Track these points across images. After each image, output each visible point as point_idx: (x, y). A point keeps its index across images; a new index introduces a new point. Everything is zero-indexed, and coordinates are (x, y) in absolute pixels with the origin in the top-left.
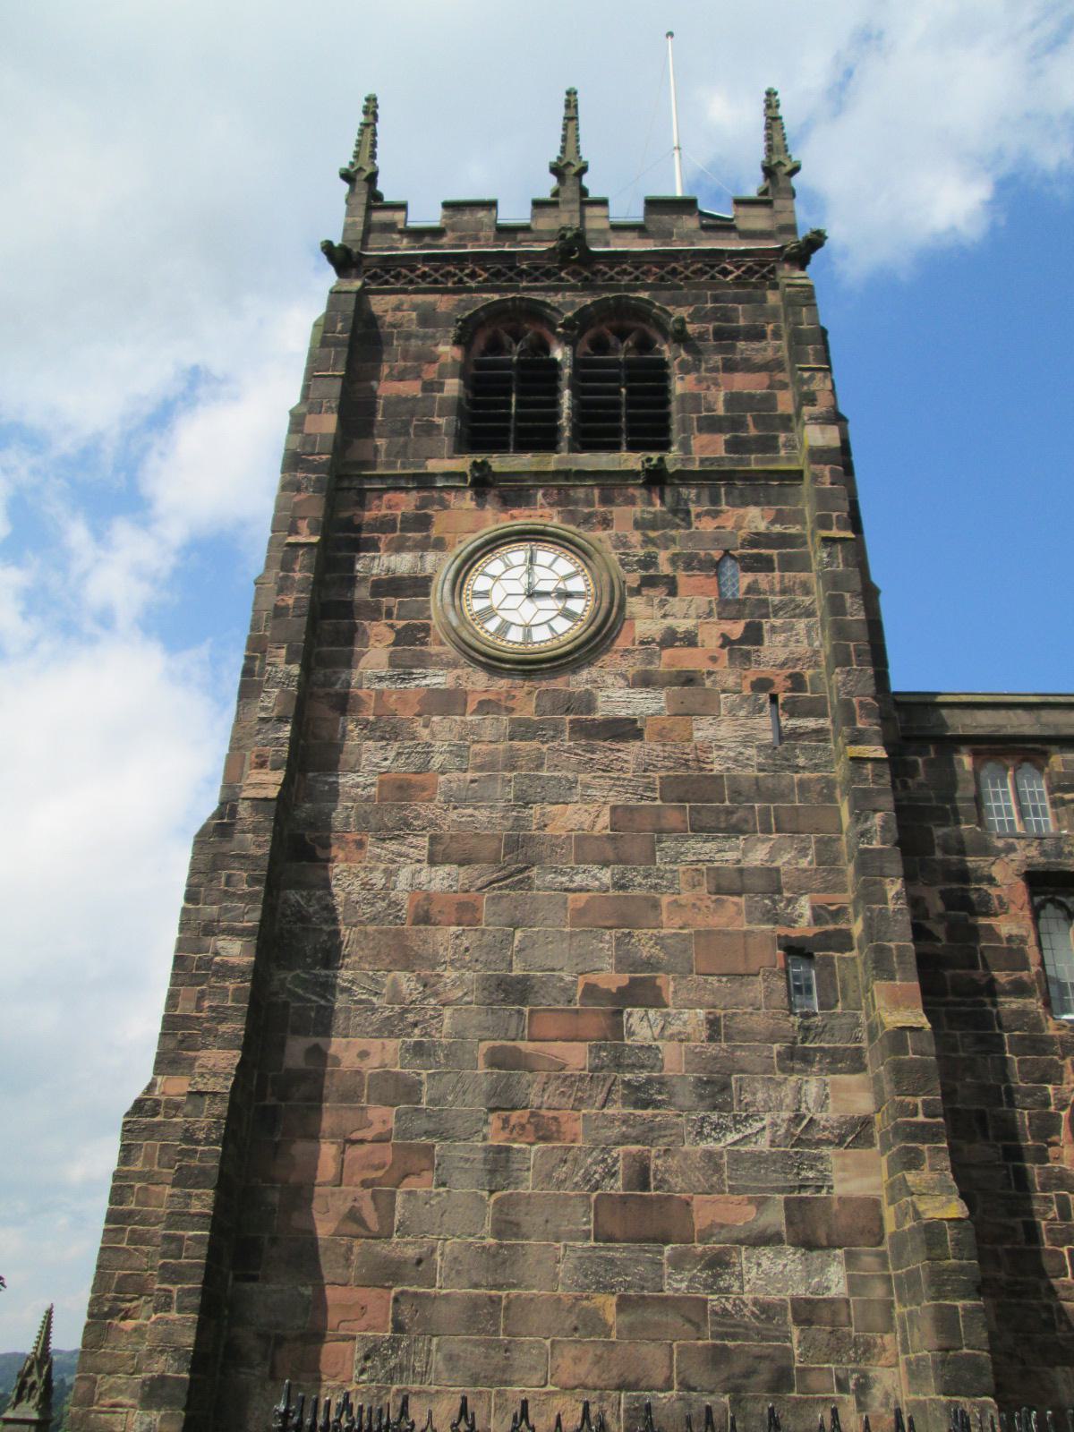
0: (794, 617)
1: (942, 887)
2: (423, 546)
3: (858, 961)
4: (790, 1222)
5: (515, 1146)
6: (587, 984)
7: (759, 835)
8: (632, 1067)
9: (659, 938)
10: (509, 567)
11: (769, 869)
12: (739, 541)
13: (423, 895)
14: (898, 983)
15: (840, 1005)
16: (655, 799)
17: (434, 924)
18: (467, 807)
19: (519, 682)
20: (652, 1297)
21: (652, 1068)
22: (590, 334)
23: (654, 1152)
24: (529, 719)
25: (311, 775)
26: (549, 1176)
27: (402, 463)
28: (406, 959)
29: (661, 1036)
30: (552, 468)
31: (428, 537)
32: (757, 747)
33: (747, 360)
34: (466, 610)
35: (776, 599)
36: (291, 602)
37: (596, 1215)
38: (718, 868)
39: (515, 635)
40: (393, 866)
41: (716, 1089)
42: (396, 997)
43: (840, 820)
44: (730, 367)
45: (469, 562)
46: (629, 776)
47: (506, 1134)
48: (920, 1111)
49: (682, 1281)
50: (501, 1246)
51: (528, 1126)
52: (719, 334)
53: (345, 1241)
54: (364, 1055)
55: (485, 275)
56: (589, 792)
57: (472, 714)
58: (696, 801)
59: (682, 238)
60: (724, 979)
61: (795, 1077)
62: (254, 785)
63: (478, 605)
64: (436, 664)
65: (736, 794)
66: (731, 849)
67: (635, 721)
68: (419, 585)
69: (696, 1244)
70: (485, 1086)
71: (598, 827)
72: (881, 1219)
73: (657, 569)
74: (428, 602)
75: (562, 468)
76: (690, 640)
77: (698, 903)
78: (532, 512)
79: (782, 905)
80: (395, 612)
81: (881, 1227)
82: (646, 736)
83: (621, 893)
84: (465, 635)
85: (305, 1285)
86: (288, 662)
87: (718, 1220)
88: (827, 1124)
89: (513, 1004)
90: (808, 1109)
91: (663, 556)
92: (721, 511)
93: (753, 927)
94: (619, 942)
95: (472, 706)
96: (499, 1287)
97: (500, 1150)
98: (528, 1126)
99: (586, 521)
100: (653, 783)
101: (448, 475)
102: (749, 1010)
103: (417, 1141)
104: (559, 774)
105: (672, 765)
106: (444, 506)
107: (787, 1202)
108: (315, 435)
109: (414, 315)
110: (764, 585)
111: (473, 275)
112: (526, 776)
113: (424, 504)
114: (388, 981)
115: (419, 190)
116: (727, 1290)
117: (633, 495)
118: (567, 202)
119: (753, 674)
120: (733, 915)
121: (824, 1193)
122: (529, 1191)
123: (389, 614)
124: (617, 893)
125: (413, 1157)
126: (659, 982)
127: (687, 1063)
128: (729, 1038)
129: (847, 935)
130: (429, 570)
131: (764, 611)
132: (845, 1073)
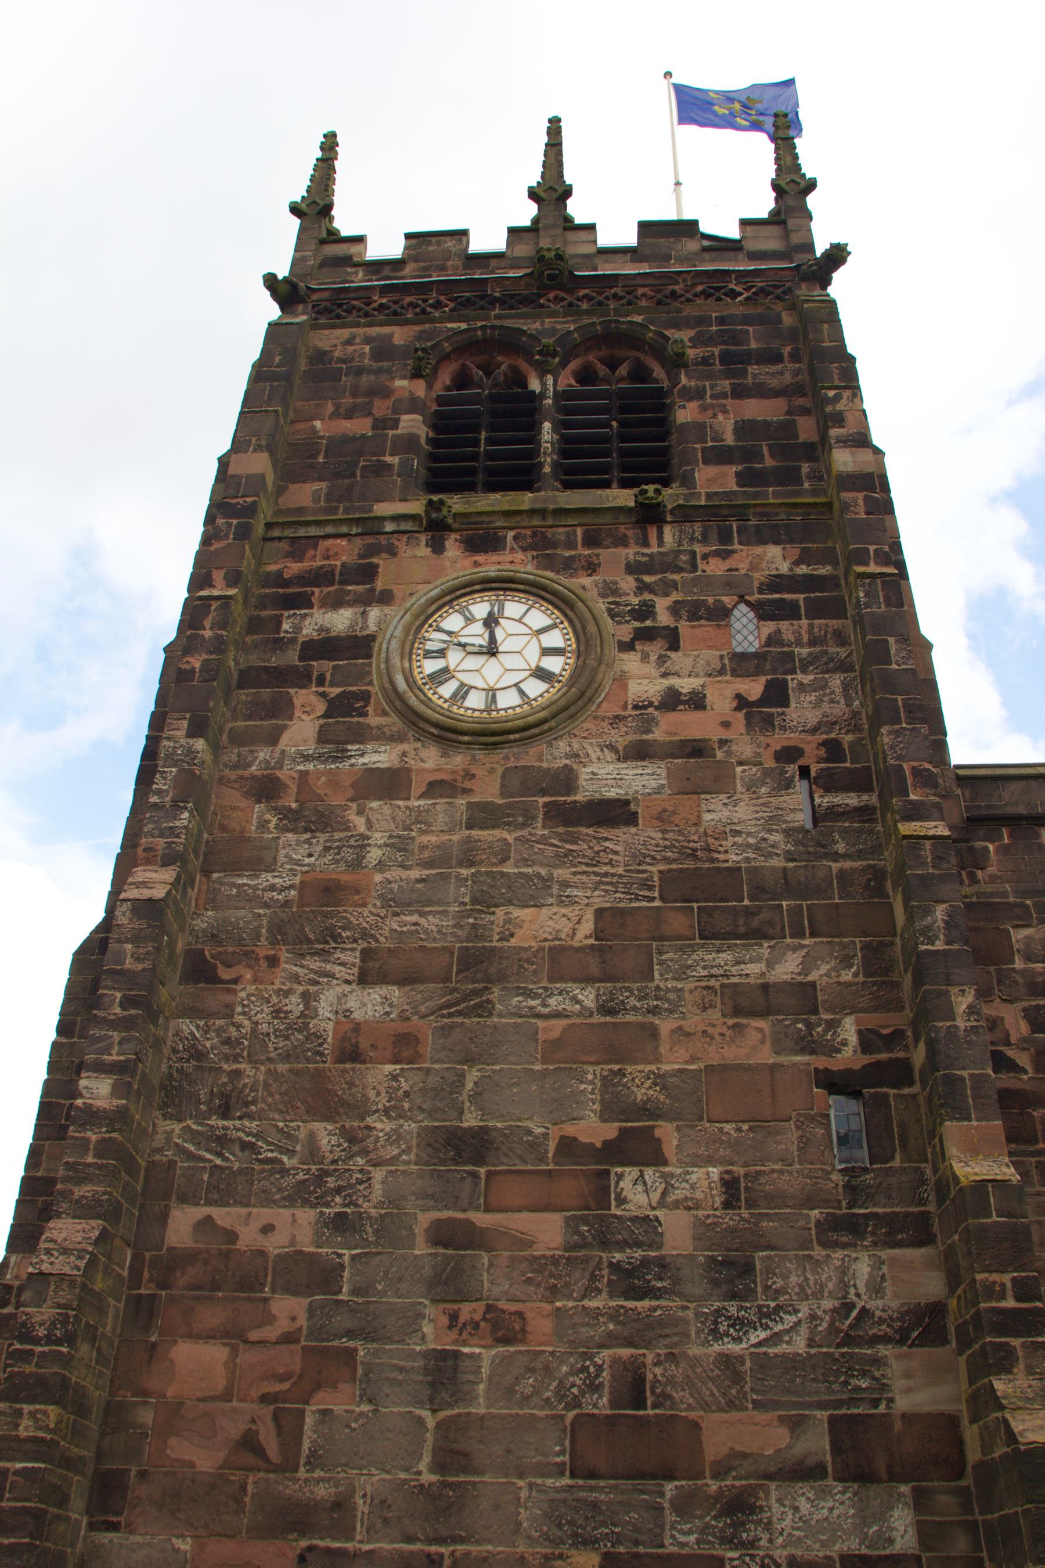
0: (827, 672)
1: (1025, 1004)
2: (366, 600)
3: (921, 1099)
4: (836, 1447)
5: (466, 1350)
6: (562, 1137)
7: (788, 940)
8: (621, 1245)
9: (658, 1076)
10: (470, 620)
11: (801, 984)
12: (756, 584)
13: (351, 1026)
14: (974, 1123)
15: (898, 1156)
16: (653, 899)
17: (364, 1062)
18: (411, 913)
19: (479, 754)
20: (647, 1554)
21: (650, 1247)
22: (574, 365)
23: (650, 1358)
24: (492, 803)
25: (216, 875)
26: (511, 1391)
27: (345, 508)
28: (326, 1104)
29: (662, 1204)
30: (526, 507)
31: (373, 590)
32: (784, 831)
33: (761, 385)
34: (416, 672)
35: (805, 651)
36: (197, 665)
37: (573, 1443)
38: (736, 984)
39: (475, 701)
40: (312, 989)
41: (733, 1271)
42: (313, 1153)
43: (894, 920)
44: (739, 393)
45: (425, 617)
46: (620, 870)
47: (453, 1335)
48: (1009, 1292)
49: (690, 1532)
50: (445, 1484)
51: (483, 1324)
52: (726, 358)
53: (236, 1477)
54: (268, 1229)
55: (452, 305)
56: (568, 892)
57: (420, 797)
58: (706, 901)
59: (680, 260)
60: (745, 1127)
61: (839, 1254)
62: (138, 885)
63: (431, 666)
64: (377, 738)
65: (759, 891)
66: (752, 961)
67: (627, 802)
68: (359, 646)
69: (709, 1482)
70: (427, 1271)
71: (579, 936)
72: (960, 1442)
73: (654, 619)
74: (370, 665)
75: (537, 506)
76: (697, 701)
77: (710, 1030)
78: (501, 559)
79: (819, 1029)
80: (328, 678)
81: (961, 1453)
82: (640, 821)
83: (608, 1019)
84: (413, 701)
85: (182, 1536)
86: (190, 735)
87: (738, 1448)
88: (885, 1315)
89: (465, 1163)
90: (858, 1295)
91: (662, 605)
92: (734, 551)
93: (785, 1059)
94: (607, 1082)
95: (418, 786)
96: (440, 1541)
97: (444, 1355)
98: (483, 1324)
99: (568, 566)
100: (651, 879)
101: (397, 518)
102: (778, 1166)
103: (336, 1343)
104: (530, 870)
105: (675, 856)
106: (392, 552)
107: (832, 1421)
108: (240, 477)
109: (367, 349)
110: (788, 635)
111: (438, 305)
112: (487, 873)
113: (371, 551)
114: (302, 1135)
115: (378, 221)
116: (753, 1543)
117: (626, 536)
118: (547, 228)
119: (779, 740)
120: (756, 1044)
121: (882, 1408)
122: (483, 1411)
123: (321, 681)
124: (603, 1019)
125: (326, 1362)
126: (657, 1133)
127: (696, 1238)
128: (750, 1204)
129: (905, 1065)
130: (372, 627)
131: (790, 666)
132: (907, 1246)
